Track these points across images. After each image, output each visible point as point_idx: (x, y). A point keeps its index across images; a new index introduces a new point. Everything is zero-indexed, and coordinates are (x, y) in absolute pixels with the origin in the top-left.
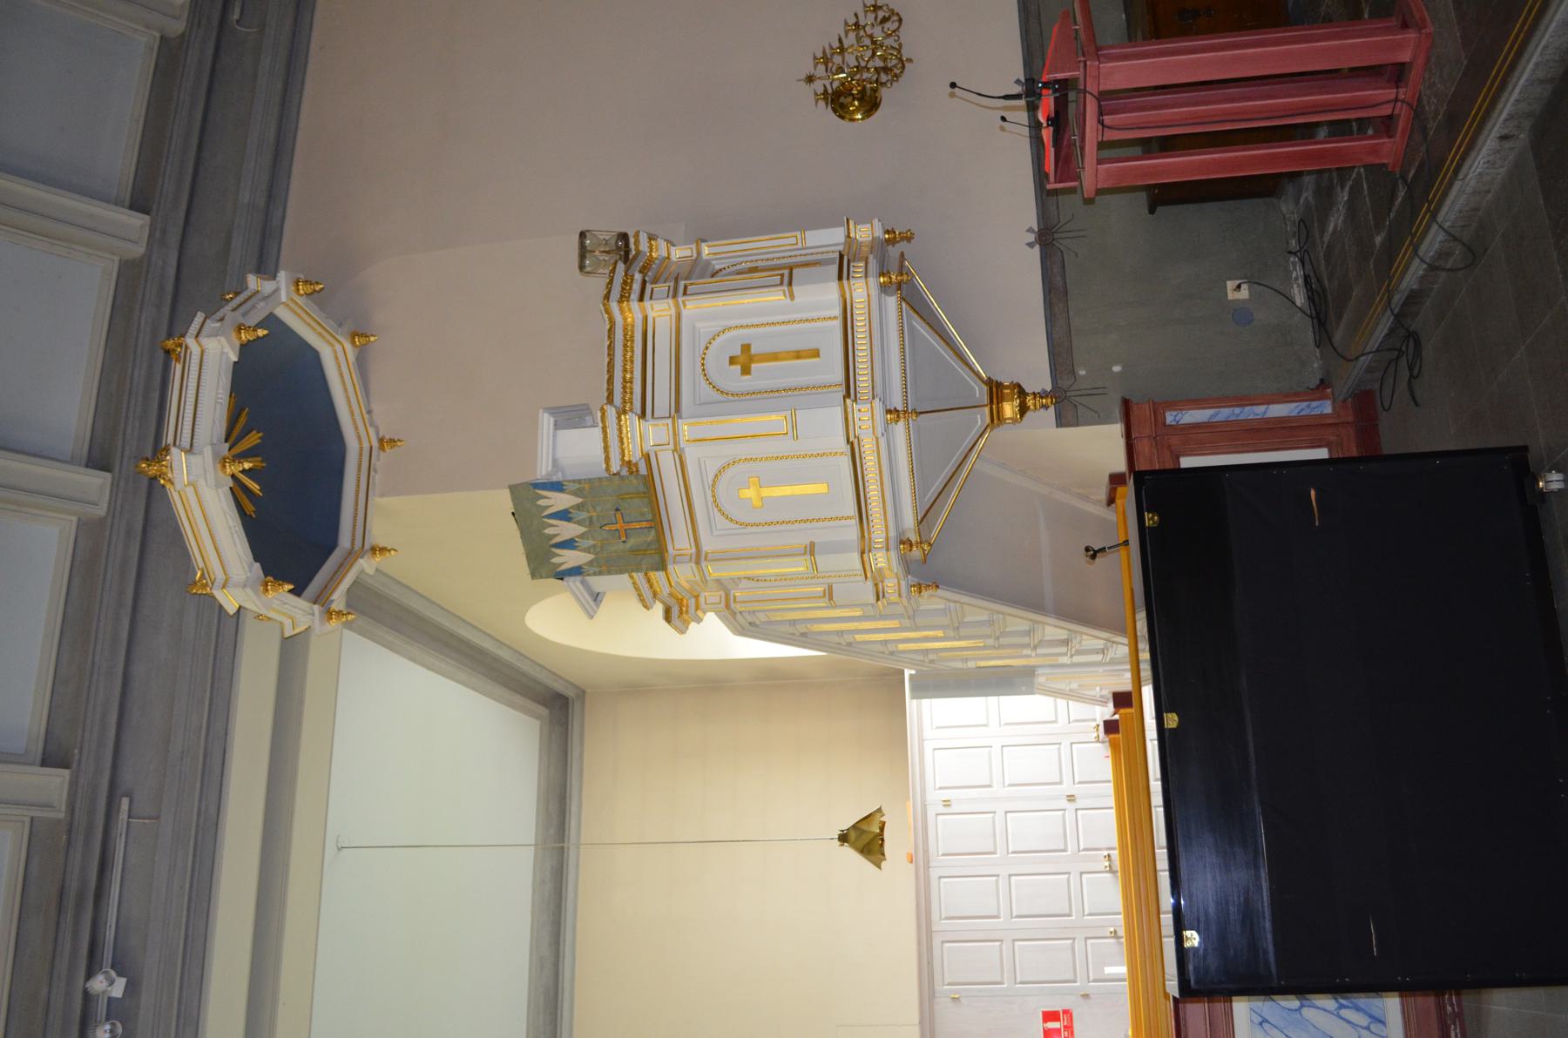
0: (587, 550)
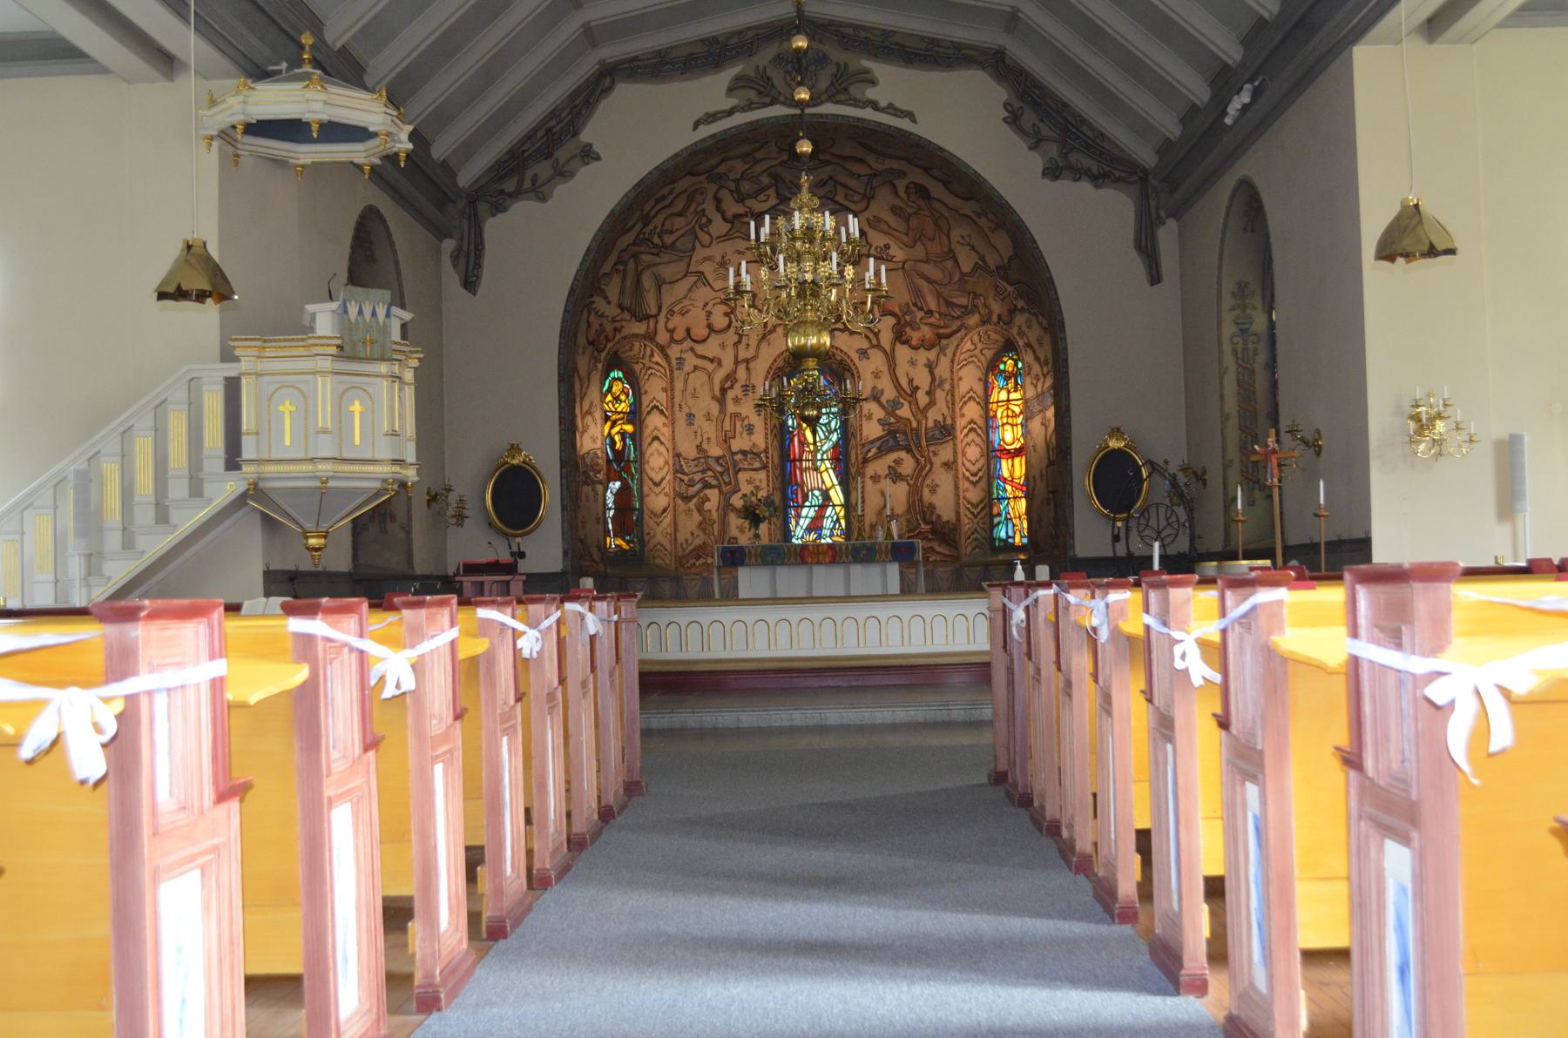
0: (357, 320)
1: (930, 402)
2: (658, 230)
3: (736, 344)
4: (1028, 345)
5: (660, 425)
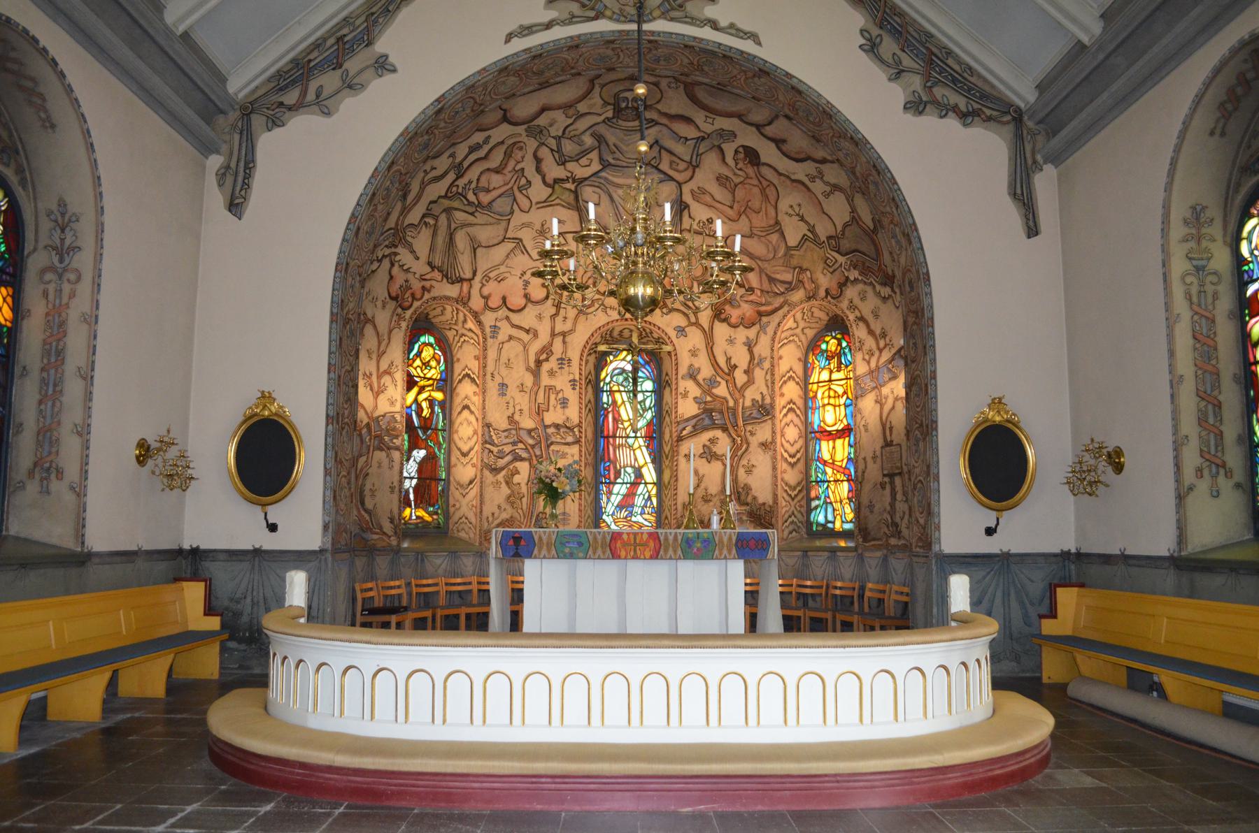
1: (748, 381)
2: (473, 185)
3: (553, 317)
4: (861, 319)
5: (470, 394)
